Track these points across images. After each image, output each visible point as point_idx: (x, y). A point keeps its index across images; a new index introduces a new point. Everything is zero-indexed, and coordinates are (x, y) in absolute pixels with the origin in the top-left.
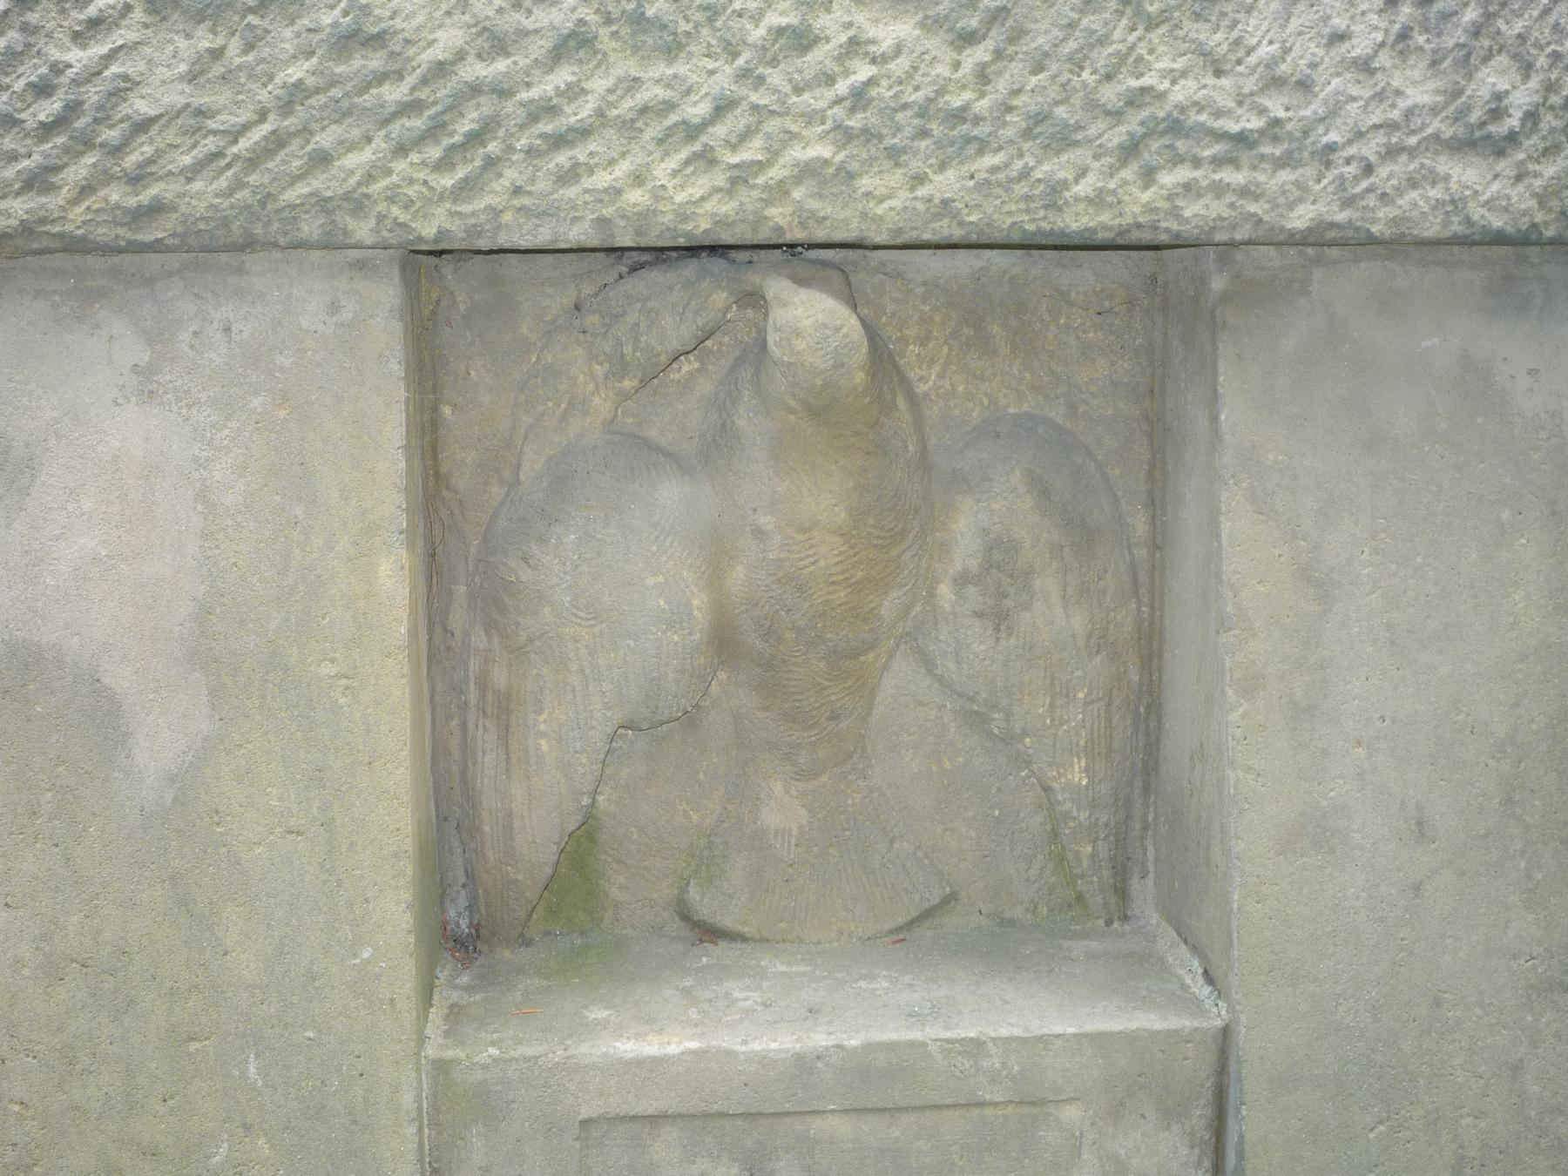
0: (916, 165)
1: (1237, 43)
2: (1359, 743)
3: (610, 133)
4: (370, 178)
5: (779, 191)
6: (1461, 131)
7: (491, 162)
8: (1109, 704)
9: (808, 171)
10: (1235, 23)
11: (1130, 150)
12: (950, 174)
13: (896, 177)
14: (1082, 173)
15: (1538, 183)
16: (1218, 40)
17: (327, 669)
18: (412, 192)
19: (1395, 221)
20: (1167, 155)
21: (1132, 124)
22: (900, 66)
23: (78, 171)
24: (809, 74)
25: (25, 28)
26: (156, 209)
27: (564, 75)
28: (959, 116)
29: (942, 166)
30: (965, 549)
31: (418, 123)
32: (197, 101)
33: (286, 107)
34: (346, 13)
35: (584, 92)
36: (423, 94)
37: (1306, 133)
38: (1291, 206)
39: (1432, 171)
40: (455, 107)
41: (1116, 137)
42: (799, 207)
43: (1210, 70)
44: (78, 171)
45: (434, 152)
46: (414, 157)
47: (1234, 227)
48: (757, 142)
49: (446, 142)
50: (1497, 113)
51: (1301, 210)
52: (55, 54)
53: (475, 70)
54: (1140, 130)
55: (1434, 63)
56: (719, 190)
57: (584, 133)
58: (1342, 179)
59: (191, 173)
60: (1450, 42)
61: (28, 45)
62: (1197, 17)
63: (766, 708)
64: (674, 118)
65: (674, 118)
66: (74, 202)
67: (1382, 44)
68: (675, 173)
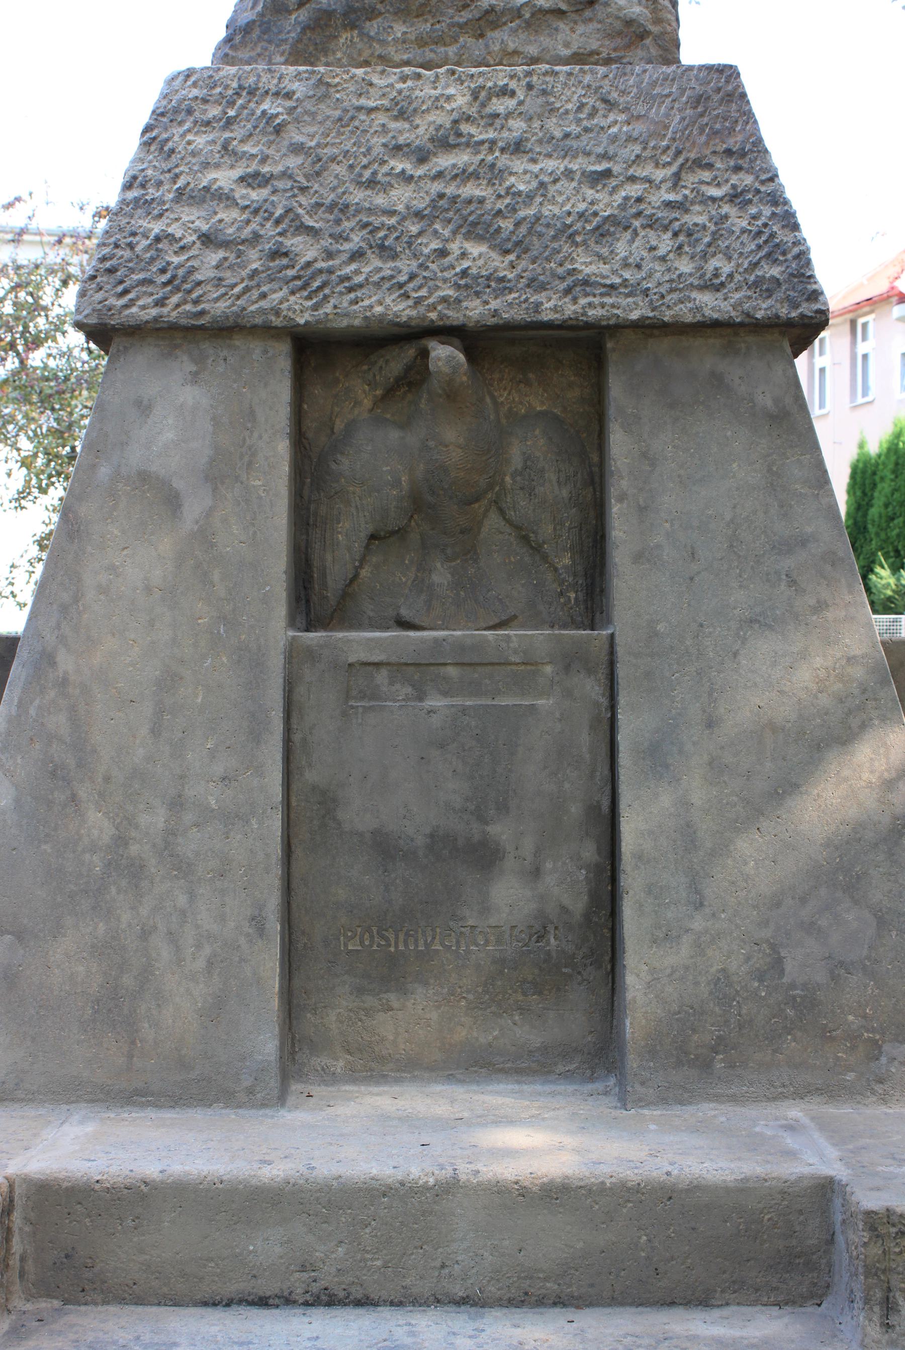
0: (485, 297)
2: (667, 521)
4: (281, 303)
5: (433, 307)
6: (702, 283)
7: (326, 297)
8: (581, 530)
9: (444, 300)
10: (612, 244)
11: (568, 291)
12: (498, 301)
13: (478, 302)
14: (550, 299)
15: (732, 300)
16: (604, 251)
17: (258, 483)
18: (297, 307)
20: (582, 293)
21: (569, 281)
22: (480, 262)
23: (175, 299)
24: (446, 265)
26: (202, 313)
27: (353, 267)
28: (502, 280)
29: (496, 298)
31: (299, 283)
32: (218, 275)
33: (251, 277)
34: (274, 245)
35: (361, 273)
36: (302, 273)
37: (639, 285)
38: (631, 311)
39: (689, 297)
40: (313, 277)
41: (563, 286)
42: (440, 312)
43: (601, 262)
44: (175, 299)
45: (306, 294)
46: (298, 295)
47: (609, 319)
49: (309, 290)
50: (716, 275)
51: (635, 312)
52: (168, 258)
54: (572, 284)
55: (692, 258)
56: (410, 307)
57: (361, 286)
59: (217, 300)
61: (158, 256)
62: (597, 243)
63: (433, 529)
64: (395, 281)
65: (395, 281)
66: (173, 310)
67: (670, 251)
68: (394, 301)
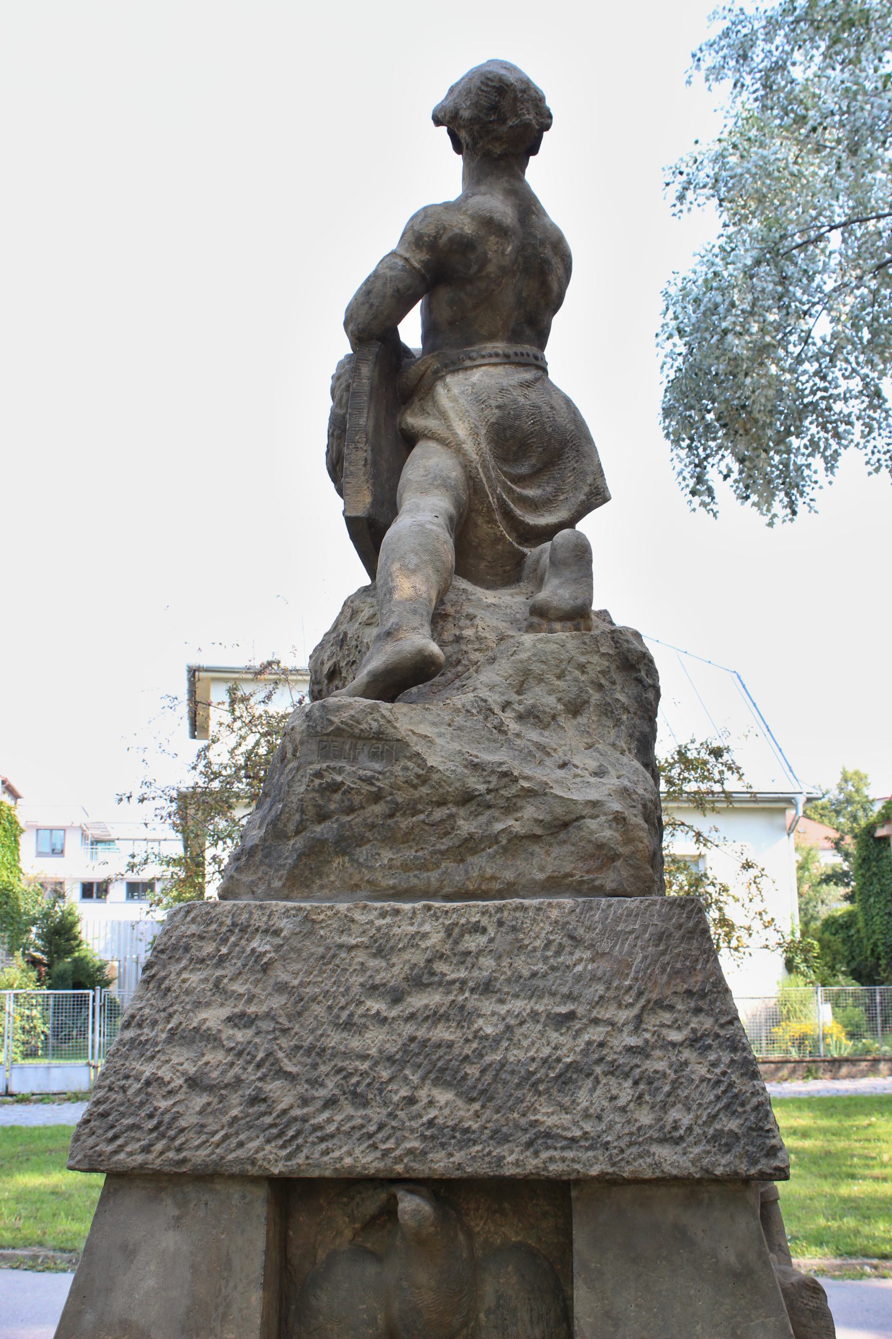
0: (450, 1149)
1: (574, 1101)
3: (342, 1136)
4: (257, 1152)
5: (399, 1160)
6: (661, 1135)
9: (410, 1152)
11: (529, 1144)
14: (512, 1152)
16: (566, 1101)
18: (271, 1157)
19: (632, 1172)
22: (446, 1112)
23: (159, 1146)
24: (414, 1113)
25: (147, 1094)
26: (184, 1161)
27: (326, 1115)
28: (467, 1130)
30: (490, 1300)
31: (275, 1131)
33: (231, 1124)
36: (277, 1121)
38: (591, 1166)
40: (288, 1125)
41: (525, 1138)
44: (159, 1146)
45: (280, 1142)
46: (273, 1144)
47: (569, 1174)
48: (392, 1140)
52: (156, 1104)
53: (297, 1112)
55: (652, 1108)
57: (332, 1136)
58: (611, 1155)
59: (198, 1147)
60: (659, 1099)
64: (365, 1130)
65: (365, 1130)
